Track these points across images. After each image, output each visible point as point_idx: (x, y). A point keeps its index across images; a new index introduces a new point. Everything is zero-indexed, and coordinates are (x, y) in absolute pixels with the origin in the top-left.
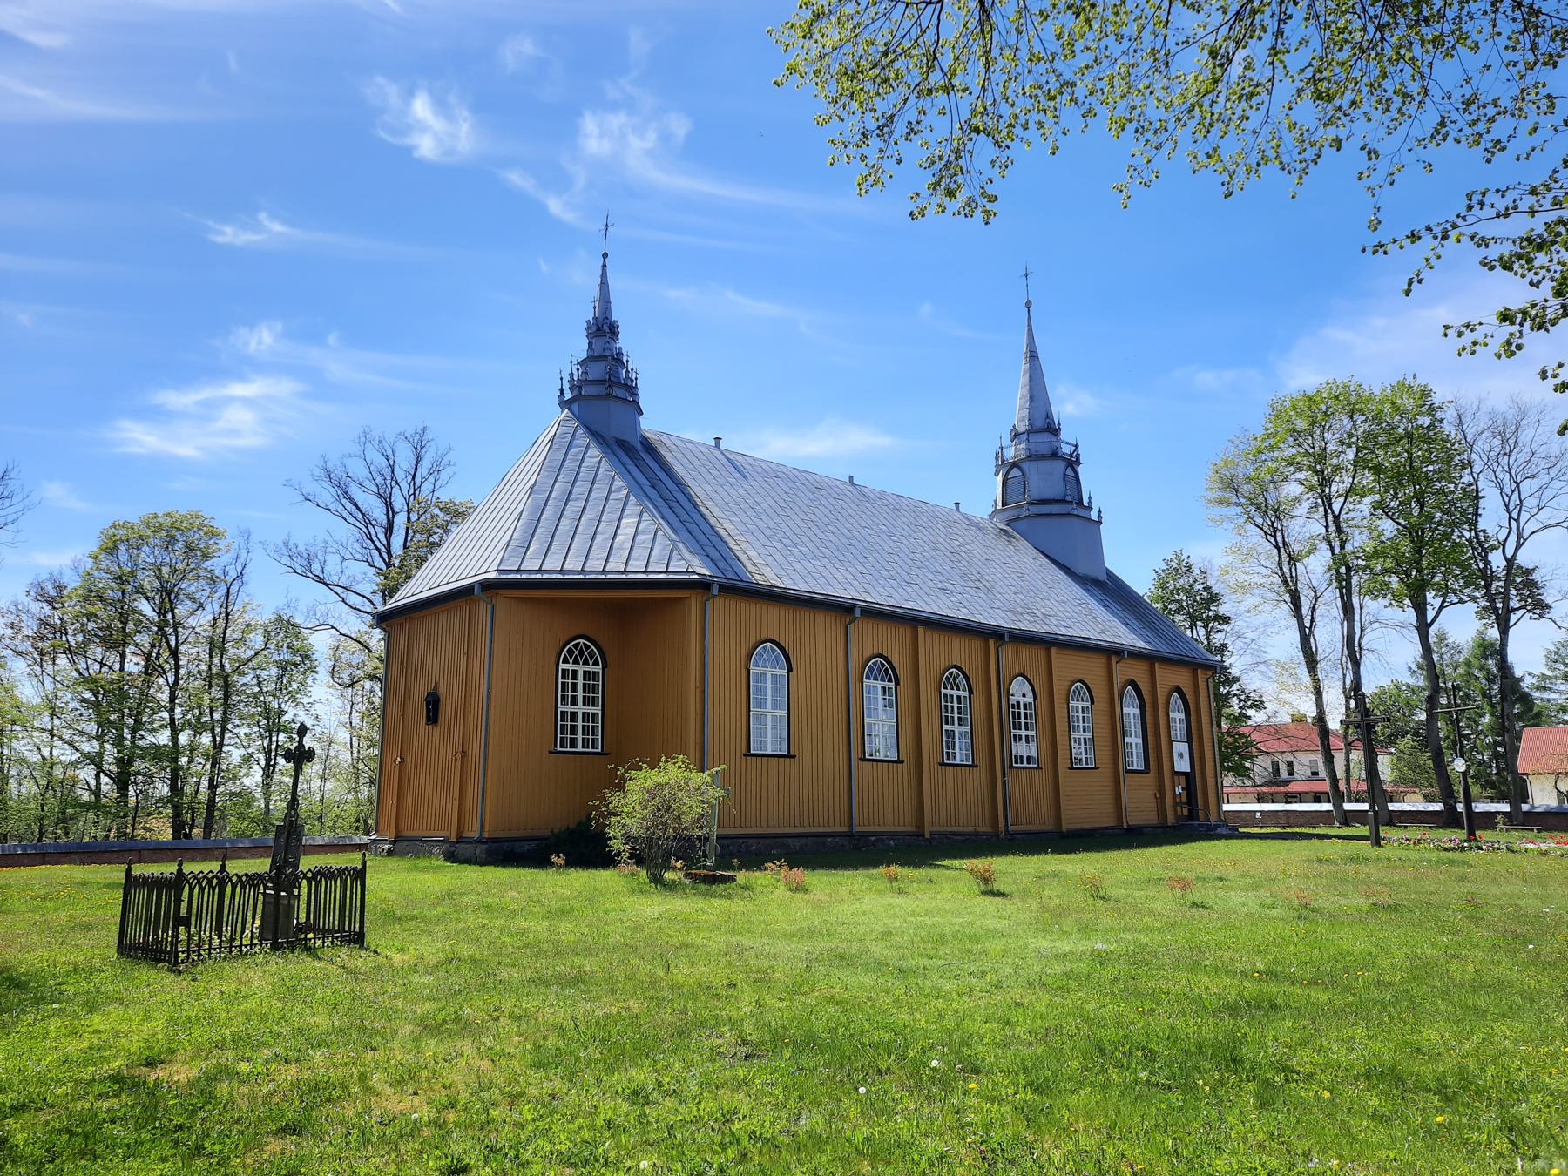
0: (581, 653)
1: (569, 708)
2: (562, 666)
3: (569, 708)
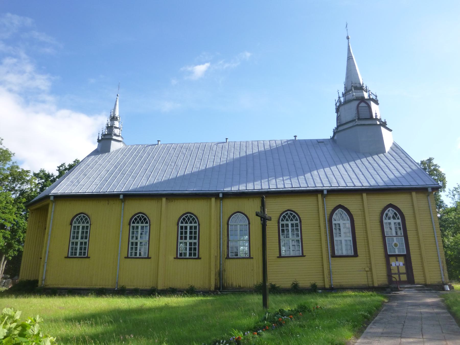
0: (289, 217)
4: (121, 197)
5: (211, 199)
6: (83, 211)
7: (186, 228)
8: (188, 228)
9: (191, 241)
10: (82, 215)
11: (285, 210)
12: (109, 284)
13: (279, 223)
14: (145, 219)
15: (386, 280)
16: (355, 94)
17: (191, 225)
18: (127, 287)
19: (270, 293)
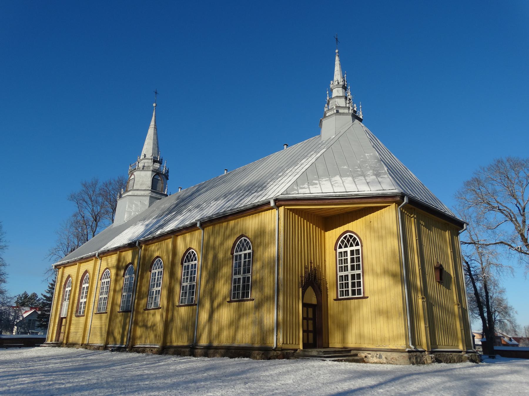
10: (348, 234)
14: (355, 239)
15: (268, 326)
16: (154, 195)
17: (352, 248)
19: (328, 347)
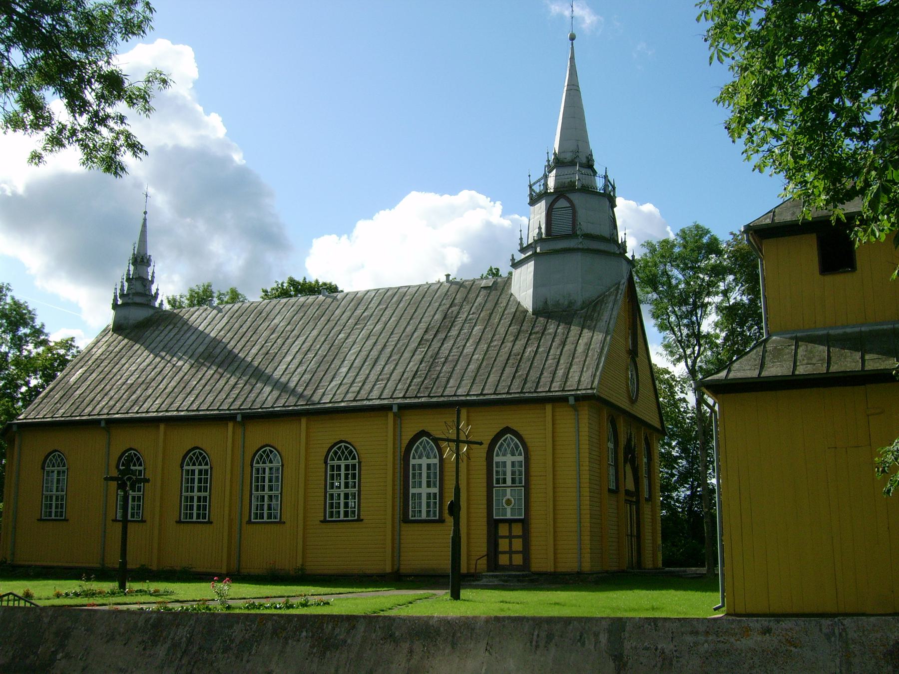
0: (343, 453)
1: (202, 494)
2: (185, 467)
3: (202, 494)
4: (103, 424)
5: (158, 427)
6: (343, 438)
7: (339, 467)
8: (197, 472)
9: (199, 494)
10: (343, 444)
11: (336, 441)
12: (287, 564)
13: (326, 463)
18: (178, 569)
